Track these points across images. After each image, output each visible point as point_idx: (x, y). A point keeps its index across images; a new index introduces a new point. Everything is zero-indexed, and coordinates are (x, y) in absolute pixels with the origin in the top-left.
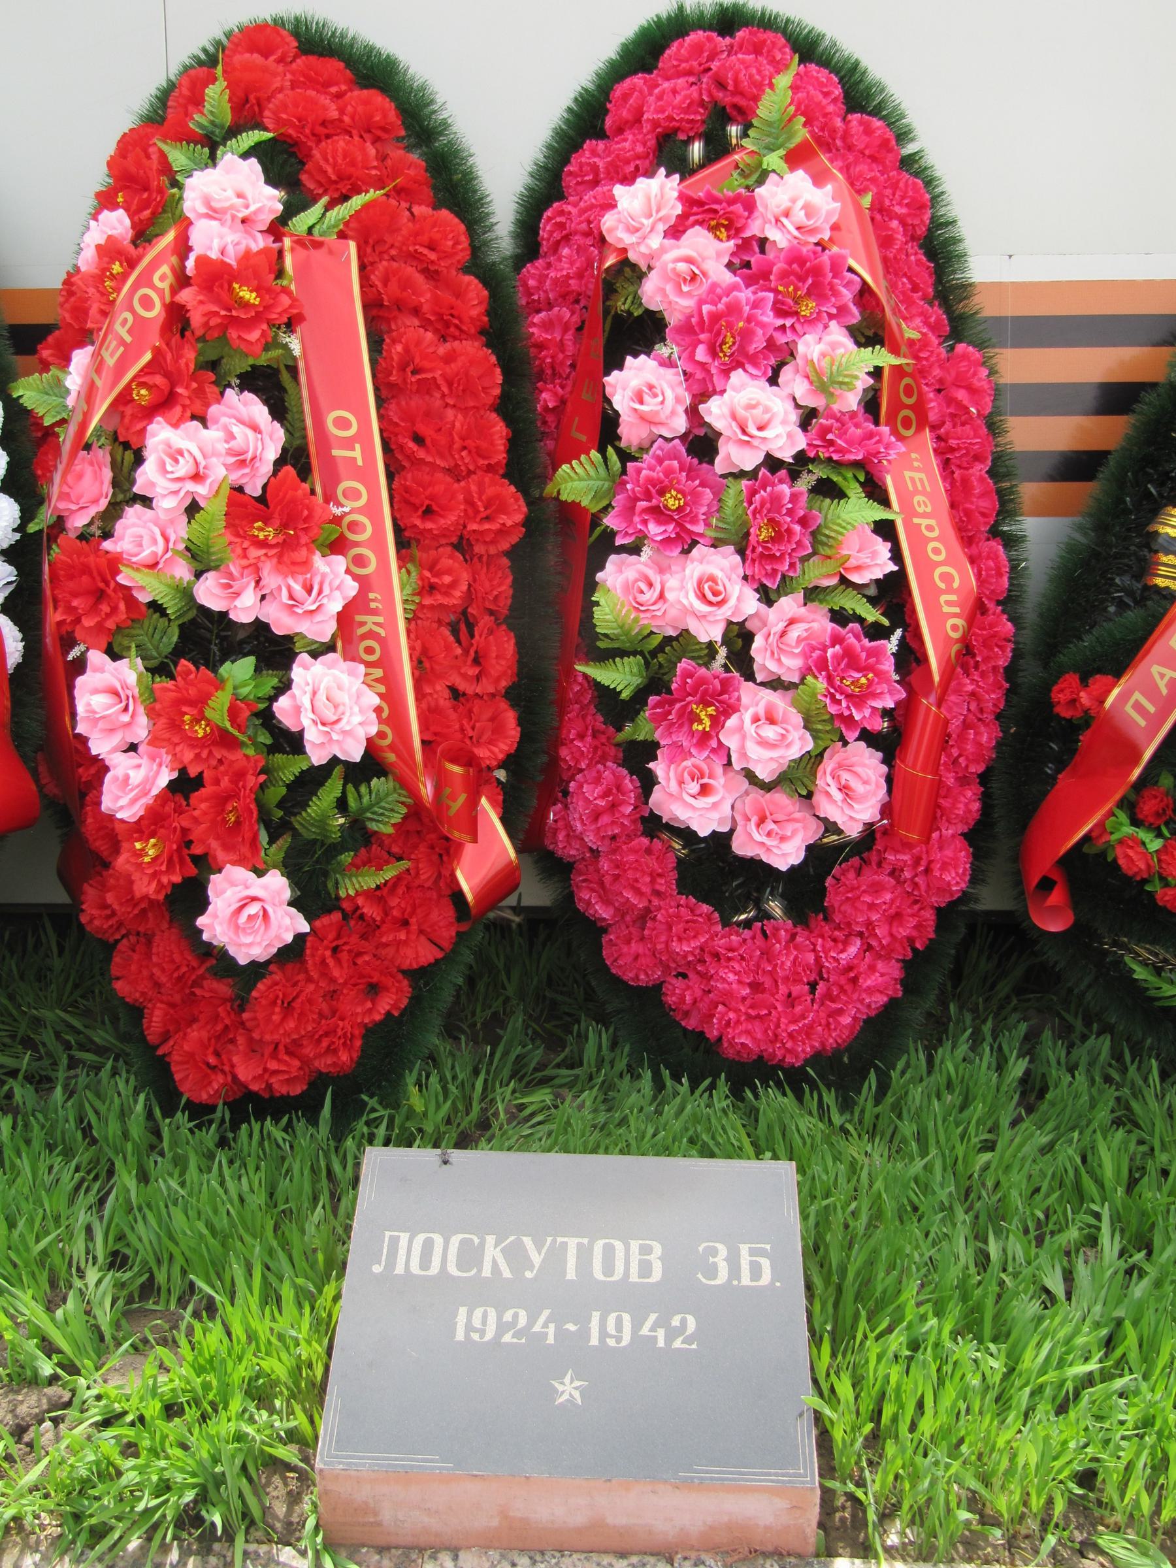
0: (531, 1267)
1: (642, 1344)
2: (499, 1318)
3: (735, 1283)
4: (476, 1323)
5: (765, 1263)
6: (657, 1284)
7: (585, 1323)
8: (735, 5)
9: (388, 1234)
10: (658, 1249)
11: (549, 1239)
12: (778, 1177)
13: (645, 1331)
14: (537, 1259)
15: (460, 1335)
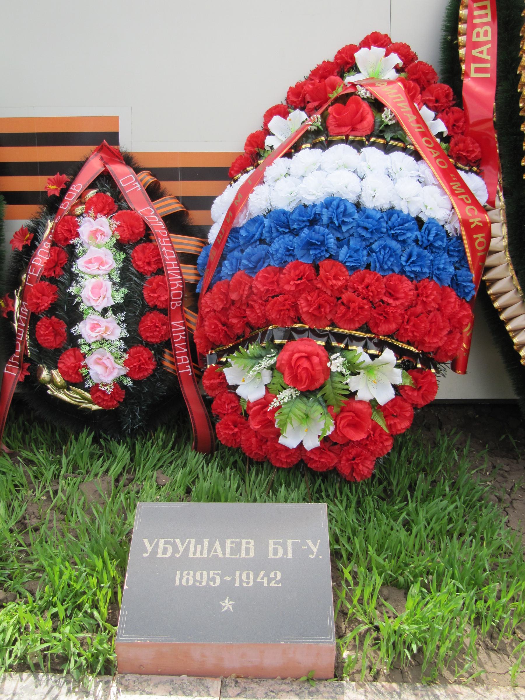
0: (178, 552)
1: (258, 585)
2: (209, 574)
3: (285, 557)
4: (184, 578)
7: (234, 575)
8: (324, 62)
10: (252, 542)
11: (188, 540)
12: (321, 509)
13: (259, 579)
14: (149, 548)
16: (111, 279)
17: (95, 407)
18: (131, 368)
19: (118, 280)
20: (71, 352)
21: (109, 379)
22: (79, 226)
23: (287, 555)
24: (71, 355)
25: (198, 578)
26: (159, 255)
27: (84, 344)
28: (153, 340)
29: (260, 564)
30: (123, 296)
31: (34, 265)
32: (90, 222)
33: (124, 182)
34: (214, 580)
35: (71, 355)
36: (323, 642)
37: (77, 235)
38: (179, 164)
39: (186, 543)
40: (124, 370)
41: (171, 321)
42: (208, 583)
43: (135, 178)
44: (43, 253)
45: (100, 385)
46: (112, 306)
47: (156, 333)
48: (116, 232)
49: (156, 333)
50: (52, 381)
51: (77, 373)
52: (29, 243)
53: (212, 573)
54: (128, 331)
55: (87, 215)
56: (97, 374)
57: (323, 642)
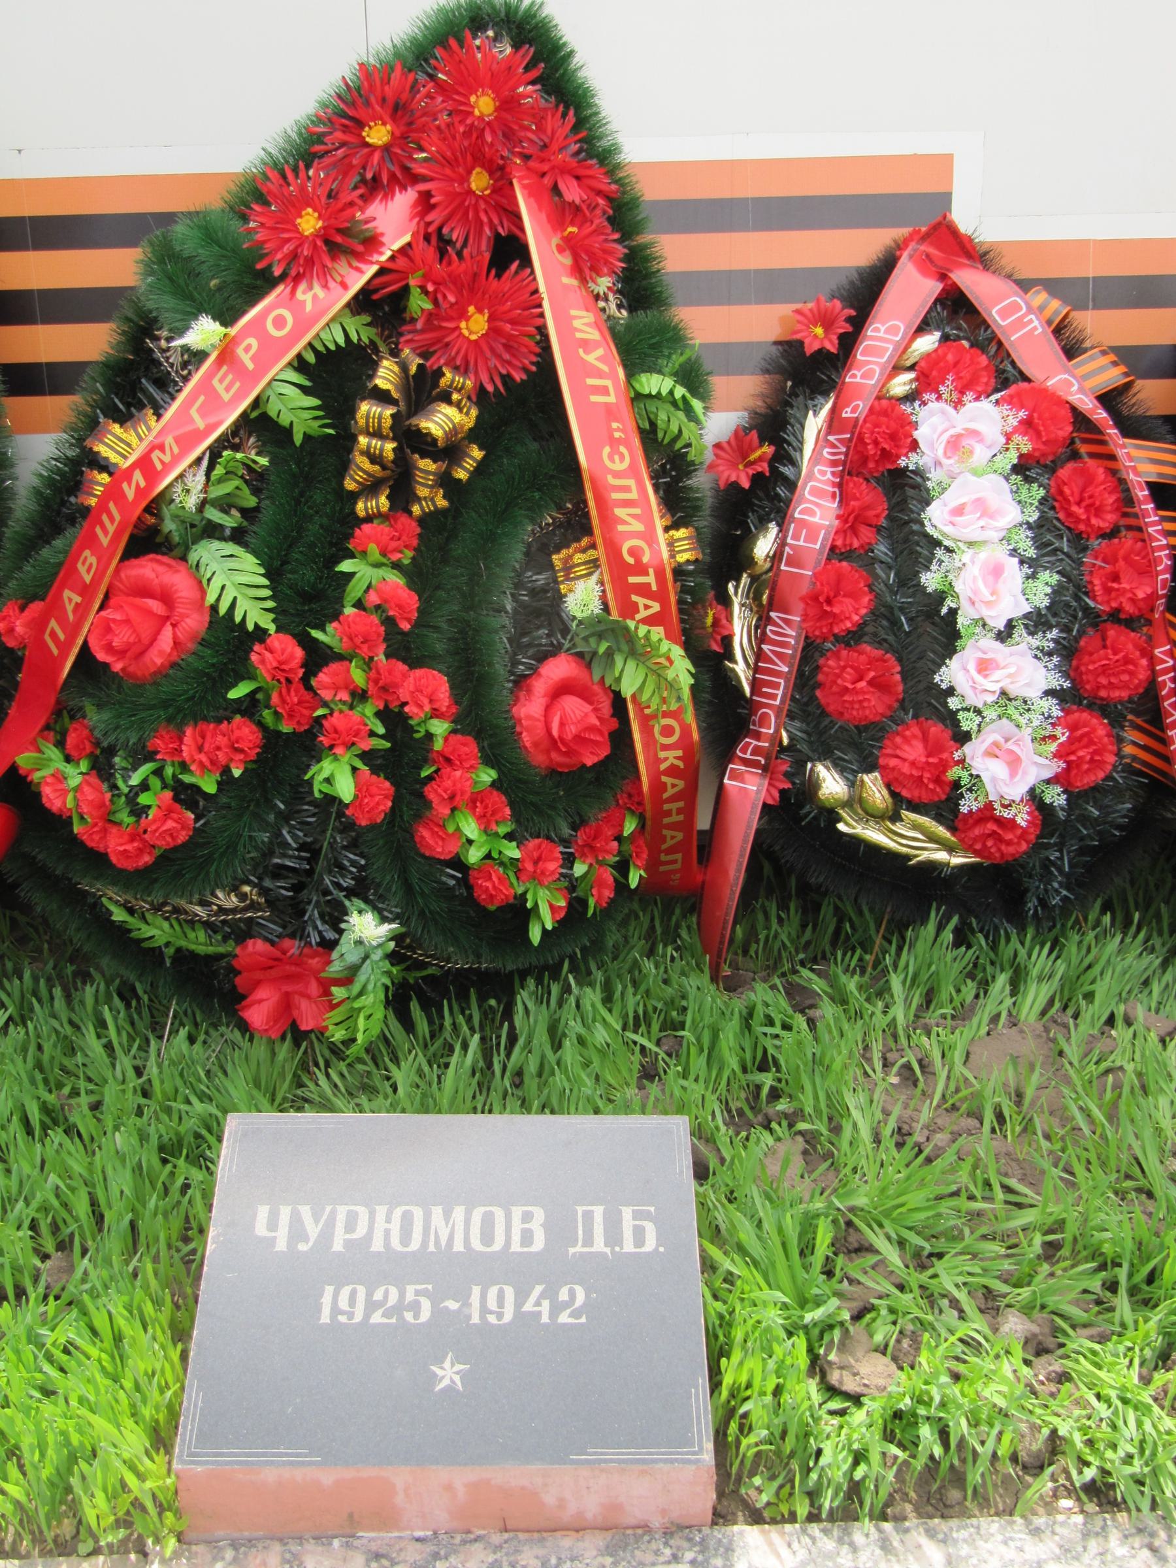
0: (306, 1239)
2: (369, 1295)
5: (650, 1229)
6: (537, 1254)
9: (580, 1210)
10: (539, 1214)
11: (328, 1209)
13: (528, 1307)
15: (325, 1318)
16: (1014, 552)
17: (957, 860)
18: (1068, 763)
19: (1031, 553)
20: (915, 730)
21: (1017, 790)
22: (915, 425)
23: (619, 1242)
24: (914, 736)
25: (343, 1304)
26: (1128, 490)
27: (964, 709)
28: (1116, 694)
29: (546, 1270)
30: (1049, 590)
31: (803, 523)
32: (943, 412)
33: (1004, 313)
34: (415, 1307)
35: (914, 736)
36: (665, 1461)
37: (914, 446)
38: (1090, 270)
39: (325, 1217)
40: (1054, 768)
41: (1153, 648)
42: (367, 1316)
43: (1027, 303)
44: (816, 492)
45: (996, 806)
46: (1027, 616)
47: (1125, 677)
48: (1017, 438)
49: (1125, 677)
50: (856, 802)
51: (938, 780)
52: (764, 467)
53: (410, 1290)
54: (1066, 675)
55: (934, 396)
56: (994, 780)
57: (665, 1461)
